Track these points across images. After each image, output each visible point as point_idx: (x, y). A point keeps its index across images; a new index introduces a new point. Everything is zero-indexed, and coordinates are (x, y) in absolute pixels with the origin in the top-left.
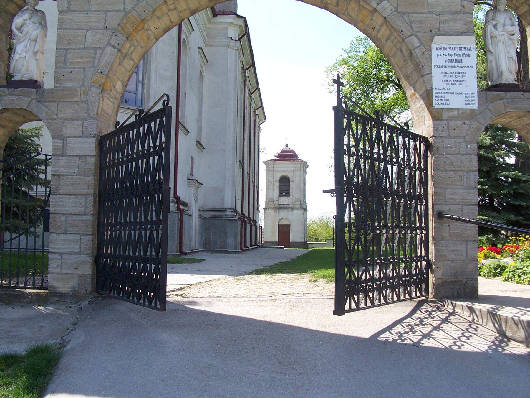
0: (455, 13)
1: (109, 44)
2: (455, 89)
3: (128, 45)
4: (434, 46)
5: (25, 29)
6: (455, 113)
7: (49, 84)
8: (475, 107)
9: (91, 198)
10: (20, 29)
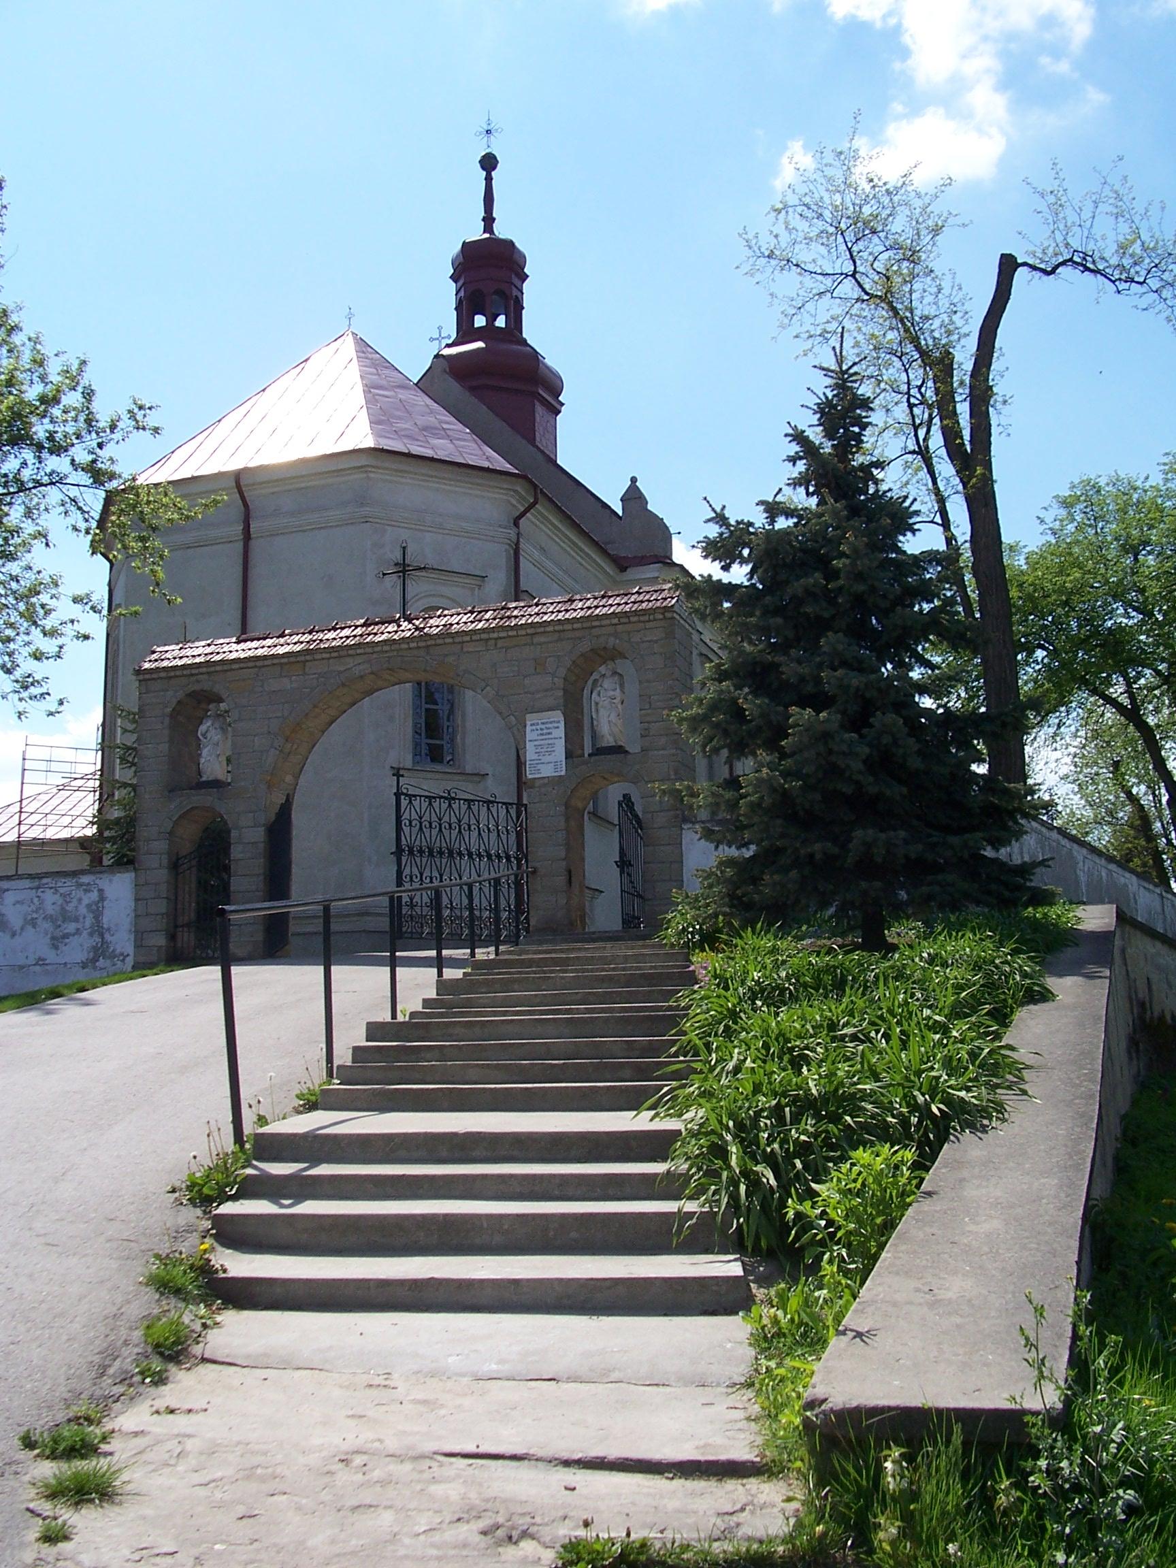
0: (547, 690)
1: (272, 747)
2: (547, 759)
3: (289, 745)
4: (528, 723)
5: (209, 735)
6: (546, 781)
7: (634, 748)
8: (563, 773)
9: (261, 878)
10: (204, 735)
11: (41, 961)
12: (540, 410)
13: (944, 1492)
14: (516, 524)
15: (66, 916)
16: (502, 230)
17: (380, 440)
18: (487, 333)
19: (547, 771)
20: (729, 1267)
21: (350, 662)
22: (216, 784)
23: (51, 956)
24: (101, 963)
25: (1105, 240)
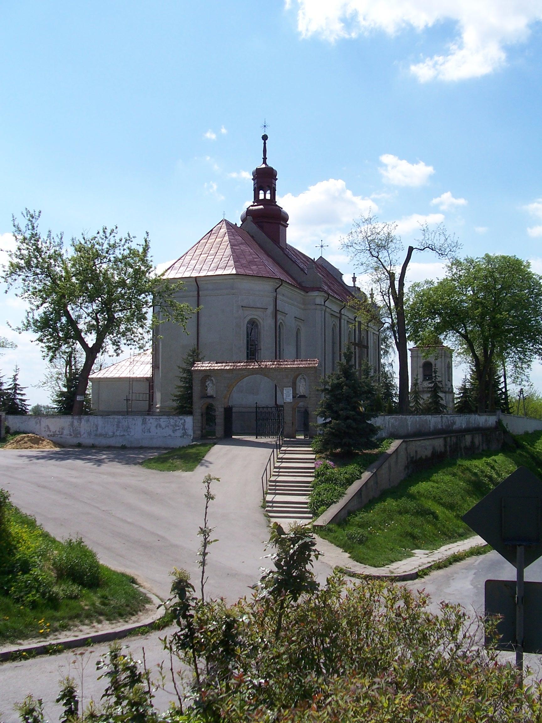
11: (170, 435)
12: (281, 227)
13: (319, 529)
14: (276, 291)
15: (176, 426)
16: (270, 163)
17: (239, 270)
18: (265, 201)
19: (288, 400)
20: (311, 515)
21: (244, 372)
22: (211, 397)
23: (172, 434)
24: (185, 437)
25: (438, 242)
